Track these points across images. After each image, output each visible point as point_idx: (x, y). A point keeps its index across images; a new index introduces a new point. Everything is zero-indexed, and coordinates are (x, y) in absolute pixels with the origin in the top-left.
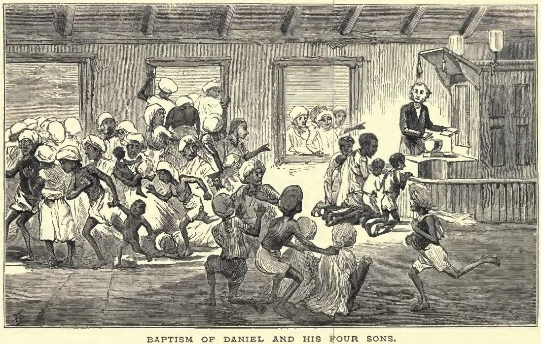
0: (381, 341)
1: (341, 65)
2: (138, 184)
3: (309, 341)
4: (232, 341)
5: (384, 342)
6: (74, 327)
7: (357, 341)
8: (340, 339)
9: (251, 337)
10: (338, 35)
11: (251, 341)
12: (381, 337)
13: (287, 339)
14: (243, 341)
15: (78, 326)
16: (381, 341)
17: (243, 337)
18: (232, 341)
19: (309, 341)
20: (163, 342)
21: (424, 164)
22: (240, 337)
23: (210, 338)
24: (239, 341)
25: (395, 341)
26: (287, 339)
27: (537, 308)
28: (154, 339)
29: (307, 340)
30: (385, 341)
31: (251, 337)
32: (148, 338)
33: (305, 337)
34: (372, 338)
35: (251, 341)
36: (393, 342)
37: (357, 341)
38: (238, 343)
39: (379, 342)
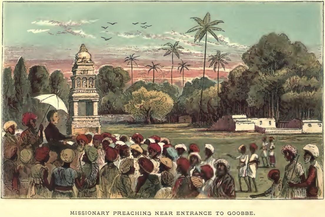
0: (93, 214)
3: (138, 214)
6: (245, 198)
7: (172, 215)
9: (161, 212)
11: (161, 214)
12: (93, 212)
15: (90, 198)
16: (93, 214)
19: (138, 214)
21: (241, 113)
22: (200, 212)
25: (254, 214)
29: (137, 214)
30: (158, 214)
31: (161, 212)
32: (177, 212)
33: (71, 212)
34: (232, 213)
35: (161, 214)
36: (253, 216)
37: (172, 215)
39: (240, 215)
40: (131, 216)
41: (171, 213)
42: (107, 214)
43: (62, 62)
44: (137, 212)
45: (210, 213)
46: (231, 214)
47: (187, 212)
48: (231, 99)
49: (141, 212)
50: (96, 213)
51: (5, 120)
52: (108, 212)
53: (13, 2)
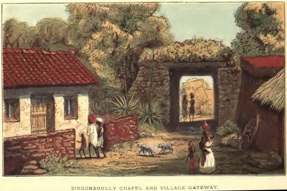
1: (93, 75)
2: (144, 136)
4: (128, 190)
5: (91, 190)
8: (87, 188)
10: (143, 74)
12: (90, 187)
13: (153, 188)
14: (152, 189)
17: (152, 187)
18: (128, 190)
20: (132, 189)
22: (150, 187)
23: (136, 187)
24: (150, 189)
26: (153, 188)
27: (3, 112)
28: (128, 188)
38: (149, 190)
40: (178, 190)
41: (155, 188)
42: (215, 188)
43: (84, 85)
44: (99, 188)
45: (183, 188)
46: (84, 189)
47: (198, 187)
48: (92, 38)
49: (102, 187)
50: (93, 188)
51: (282, 49)
52: (216, 186)
53: (60, 3)
